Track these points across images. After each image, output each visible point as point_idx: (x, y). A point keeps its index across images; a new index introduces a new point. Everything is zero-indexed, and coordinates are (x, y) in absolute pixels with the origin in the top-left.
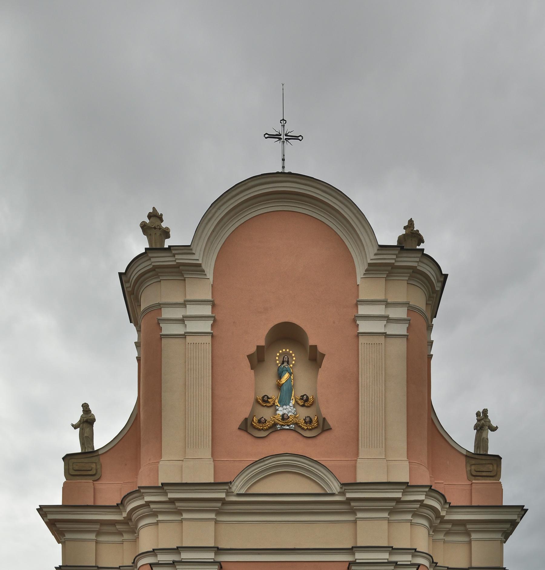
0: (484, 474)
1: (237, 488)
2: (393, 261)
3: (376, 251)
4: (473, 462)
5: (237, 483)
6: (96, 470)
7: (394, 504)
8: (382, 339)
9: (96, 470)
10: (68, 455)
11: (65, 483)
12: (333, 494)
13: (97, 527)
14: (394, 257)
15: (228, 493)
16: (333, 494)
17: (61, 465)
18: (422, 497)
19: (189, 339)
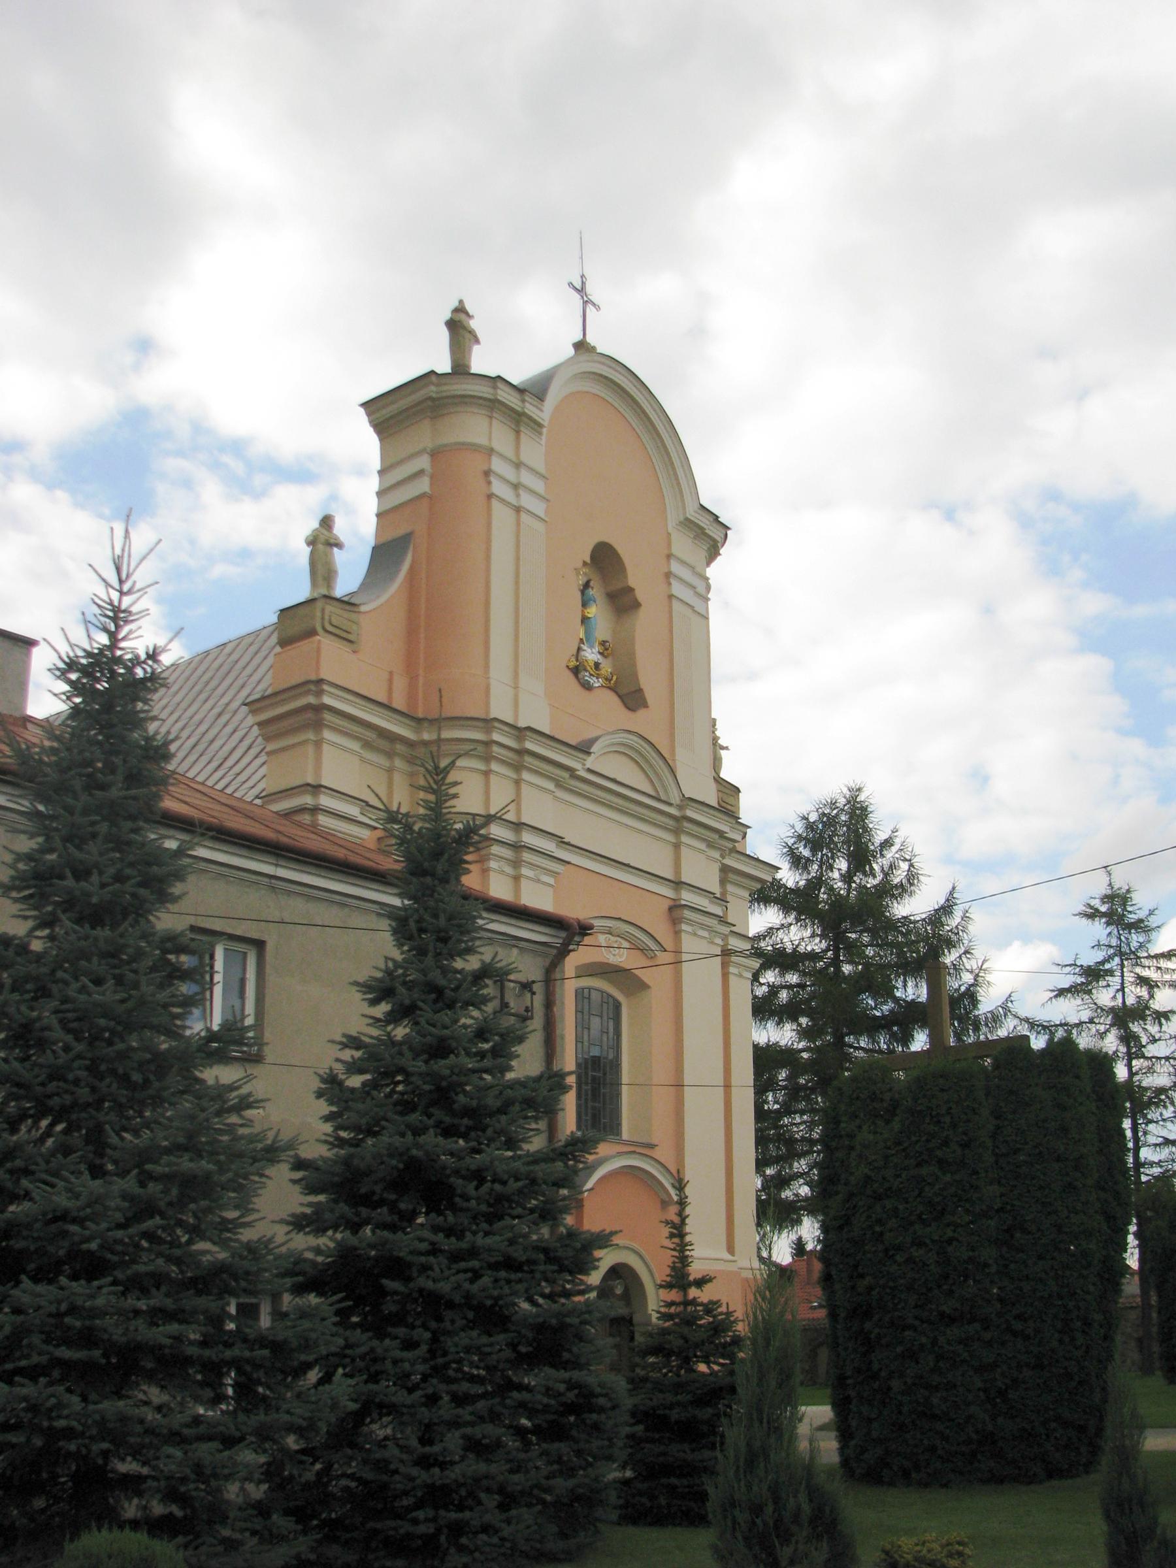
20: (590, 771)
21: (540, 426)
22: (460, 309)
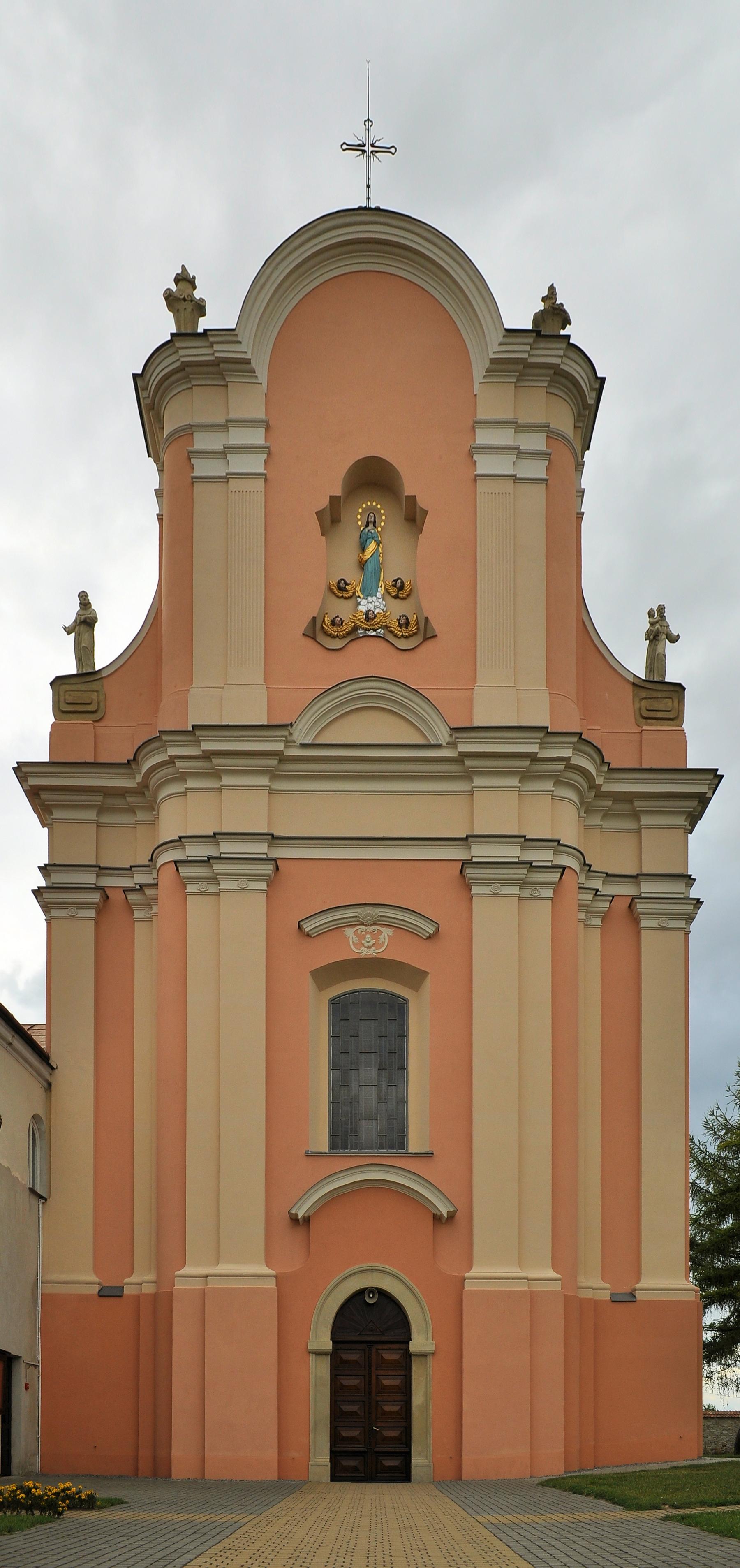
0: (659, 715)
1: (301, 734)
2: (525, 356)
3: (501, 339)
4: (644, 694)
5: (300, 726)
6: (98, 703)
7: (527, 763)
8: (509, 485)
9: (98, 703)
10: (58, 679)
11: (53, 725)
12: (439, 746)
13: (98, 799)
14: (528, 348)
15: (288, 743)
16: (439, 746)
17: (48, 694)
18: (567, 753)
19: (233, 484)
20: (304, 746)
21: (248, 362)
22: (184, 279)
